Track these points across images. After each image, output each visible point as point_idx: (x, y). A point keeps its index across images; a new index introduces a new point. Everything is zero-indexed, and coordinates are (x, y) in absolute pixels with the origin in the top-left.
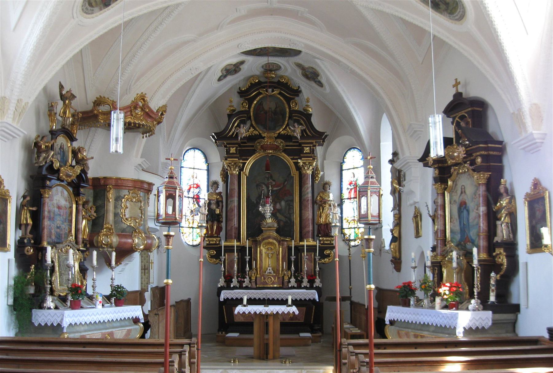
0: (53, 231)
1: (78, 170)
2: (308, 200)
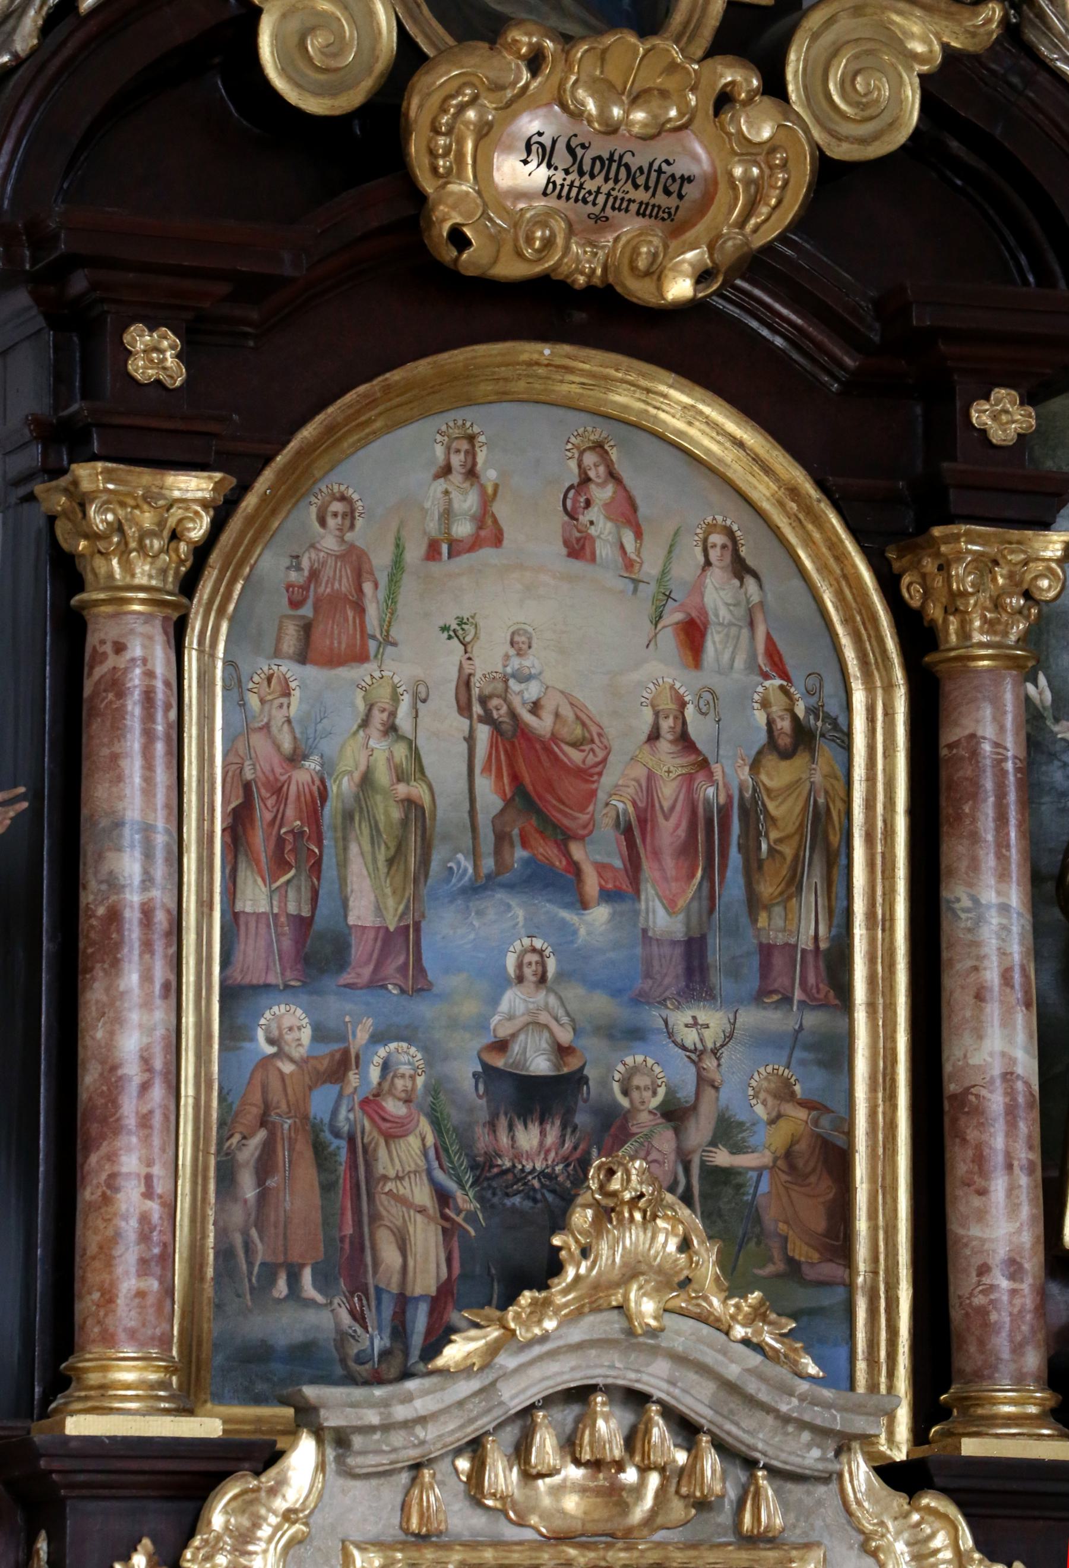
0: (406, 1163)
2: (978, 1111)
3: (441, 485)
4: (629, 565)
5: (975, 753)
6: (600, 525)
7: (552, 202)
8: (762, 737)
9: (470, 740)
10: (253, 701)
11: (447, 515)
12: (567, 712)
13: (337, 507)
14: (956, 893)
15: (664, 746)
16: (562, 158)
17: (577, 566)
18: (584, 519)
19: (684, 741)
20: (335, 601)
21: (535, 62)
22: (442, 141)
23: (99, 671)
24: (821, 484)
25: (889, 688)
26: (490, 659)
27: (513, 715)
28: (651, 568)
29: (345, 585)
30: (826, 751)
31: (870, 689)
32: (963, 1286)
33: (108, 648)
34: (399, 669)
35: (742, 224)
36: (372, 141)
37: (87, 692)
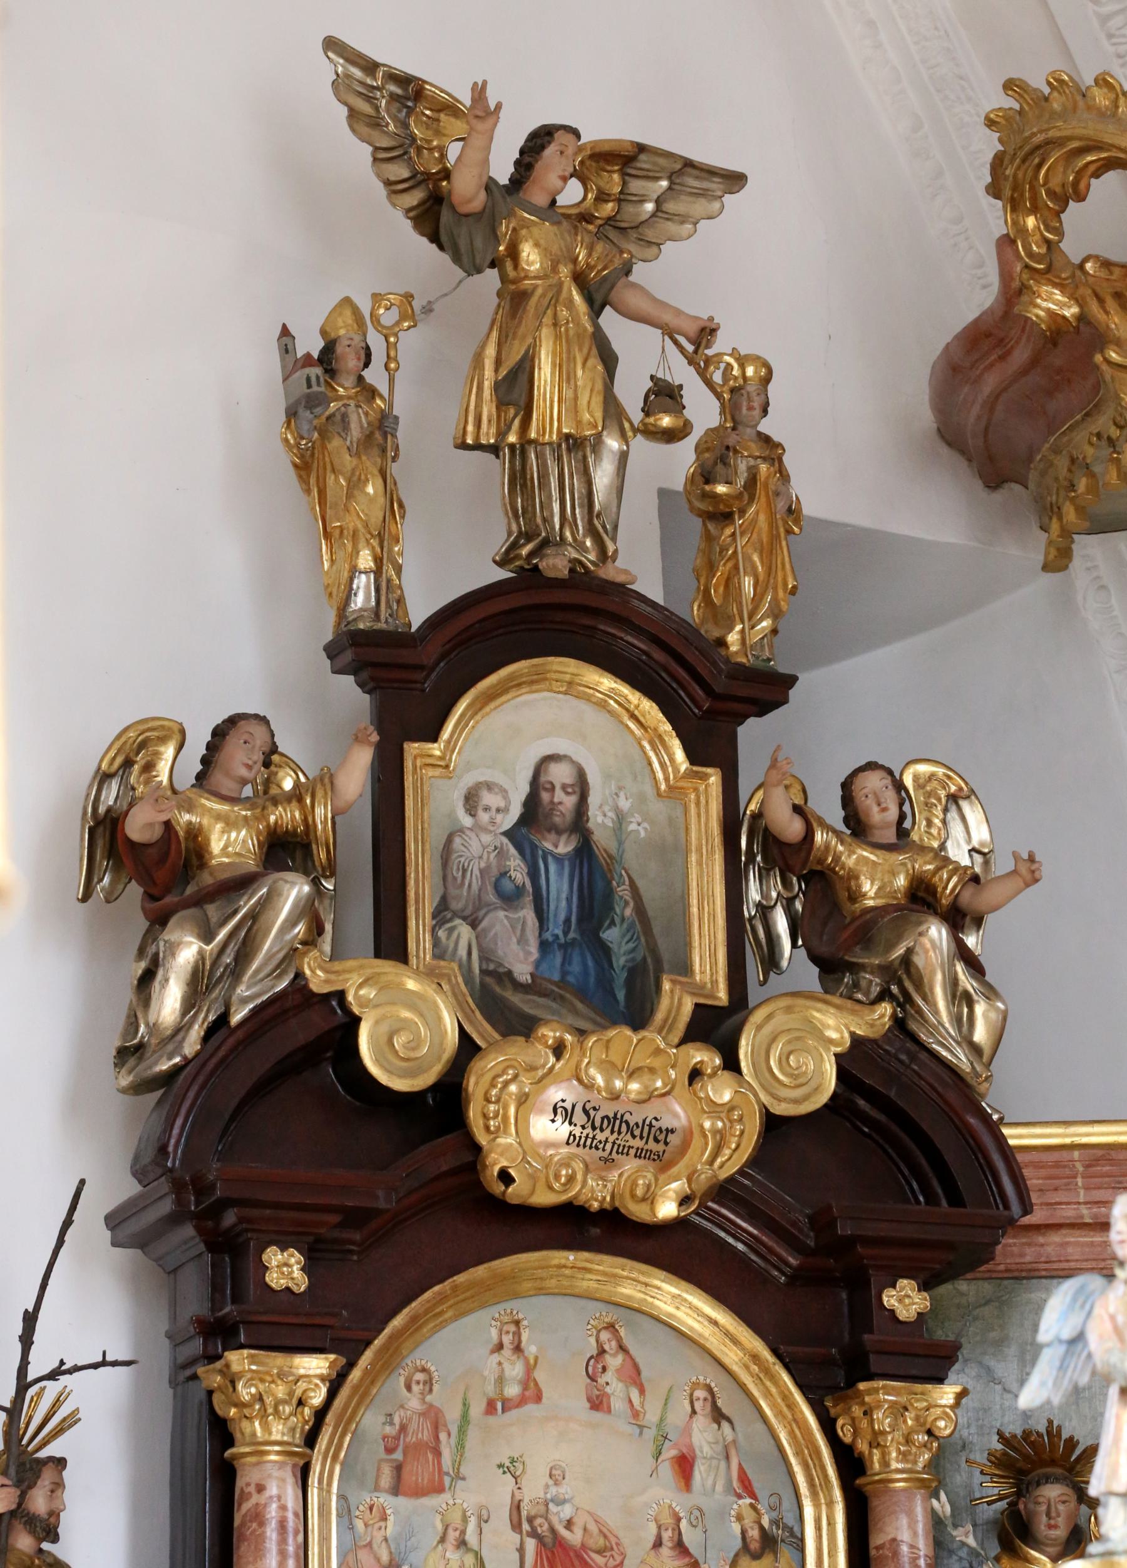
1: (803, 1047)
3: (496, 1358)
4: (636, 1414)
5: (896, 1554)
6: (615, 1386)
7: (573, 1149)
8: (738, 1544)
9: (521, 1550)
10: (359, 1525)
11: (501, 1380)
12: (593, 1528)
13: (419, 1376)
15: (665, 1551)
16: (579, 1117)
17: (597, 1416)
18: (601, 1380)
19: (680, 1547)
20: (417, 1449)
21: (558, 1050)
22: (492, 1107)
23: (246, 1506)
24: (775, 1352)
25: (830, 1504)
26: (534, 1489)
27: (553, 1530)
28: (652, 1416)
29: (426, 1435)
30: (786, 1553)
31: (817, 1505)
33: (252, 1489)
34: (466, 1497)
35: (711, 1162)
36: (442, 1106)
37: (237, 1522)
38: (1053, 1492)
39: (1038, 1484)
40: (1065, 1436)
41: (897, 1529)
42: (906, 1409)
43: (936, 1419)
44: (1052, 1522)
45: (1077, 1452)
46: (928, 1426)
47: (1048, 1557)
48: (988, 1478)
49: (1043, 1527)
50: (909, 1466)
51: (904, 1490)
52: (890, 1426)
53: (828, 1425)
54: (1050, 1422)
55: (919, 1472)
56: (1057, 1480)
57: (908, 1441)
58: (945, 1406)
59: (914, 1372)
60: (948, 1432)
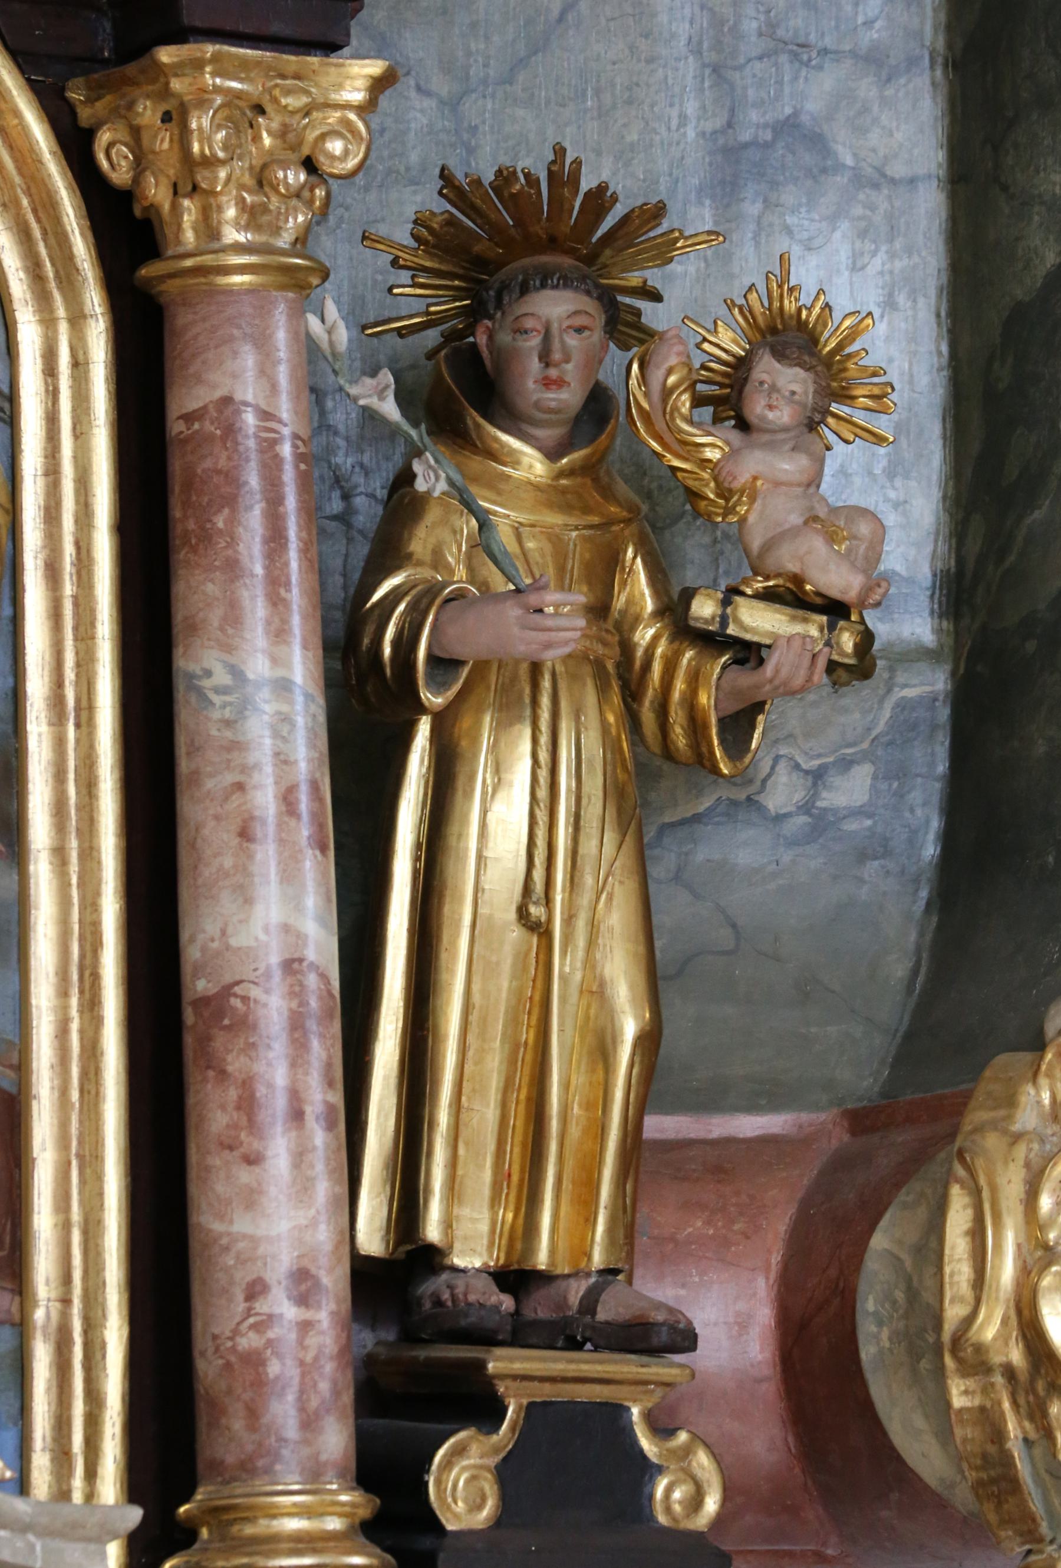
2: (244, 1025)
5: (230, 431)
14: (200, 662)
25: (78, 319)
31: (48, 322)
32: (219, 1321)
38: (555, 307)
39: (525, 290)
40: (586, 184)
41: (234, 376)
42: (260, 110)
43: (323, 137)
44: (553, 373)
45: (609, 222)
46: (306, 151)
47: (539, 449)
48: (405, 276)
49: (531, 385)
50: (261, 238)
51: (251, 291)
52: (225, 148)
53: (76, 145)
54: (560, 151)
55: (283, 253)
56: (566, 282)
57: (262, 181)
58: (347, 106)
59: (276, 28)
60: (351, 164)
